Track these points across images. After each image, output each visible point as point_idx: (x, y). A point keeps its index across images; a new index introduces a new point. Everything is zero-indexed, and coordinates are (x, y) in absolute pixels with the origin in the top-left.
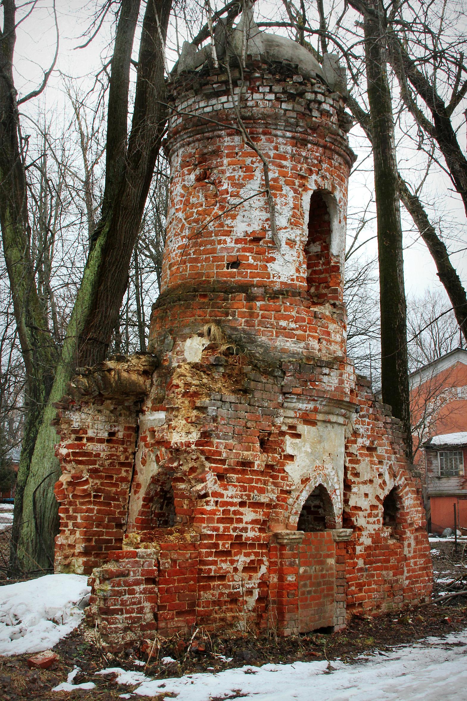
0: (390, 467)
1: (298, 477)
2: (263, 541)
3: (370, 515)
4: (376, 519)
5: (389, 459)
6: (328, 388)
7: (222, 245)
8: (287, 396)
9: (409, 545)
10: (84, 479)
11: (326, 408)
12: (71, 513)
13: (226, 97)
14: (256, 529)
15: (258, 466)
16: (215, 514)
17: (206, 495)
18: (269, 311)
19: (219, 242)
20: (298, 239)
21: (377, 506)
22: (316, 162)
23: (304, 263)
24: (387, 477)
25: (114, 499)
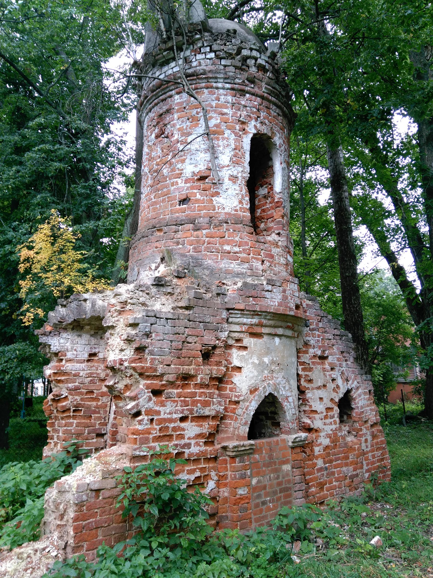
0: (342, 373)
1: (247, 387)
2: (210, 455)
3: (326, 417)
4: (332, 420)
5: (341, 366)
6: (272, 304)
7: (175, 187)
8: (231, 311)
9: (366, 441)
10: (63, 396)
11: (271, 322)
12: (56, 427)
13: (174, 62)
14: (201, 444)
15: (202, 379)
16: (150, 433)
17: (138, 414)
18: (213, 237)
19: (173, 185)
20: (240, 175)
21: (333, 408)
22: (255, 110)
23: (246, 196)
24: (340, 382)
25: (95, 412)
